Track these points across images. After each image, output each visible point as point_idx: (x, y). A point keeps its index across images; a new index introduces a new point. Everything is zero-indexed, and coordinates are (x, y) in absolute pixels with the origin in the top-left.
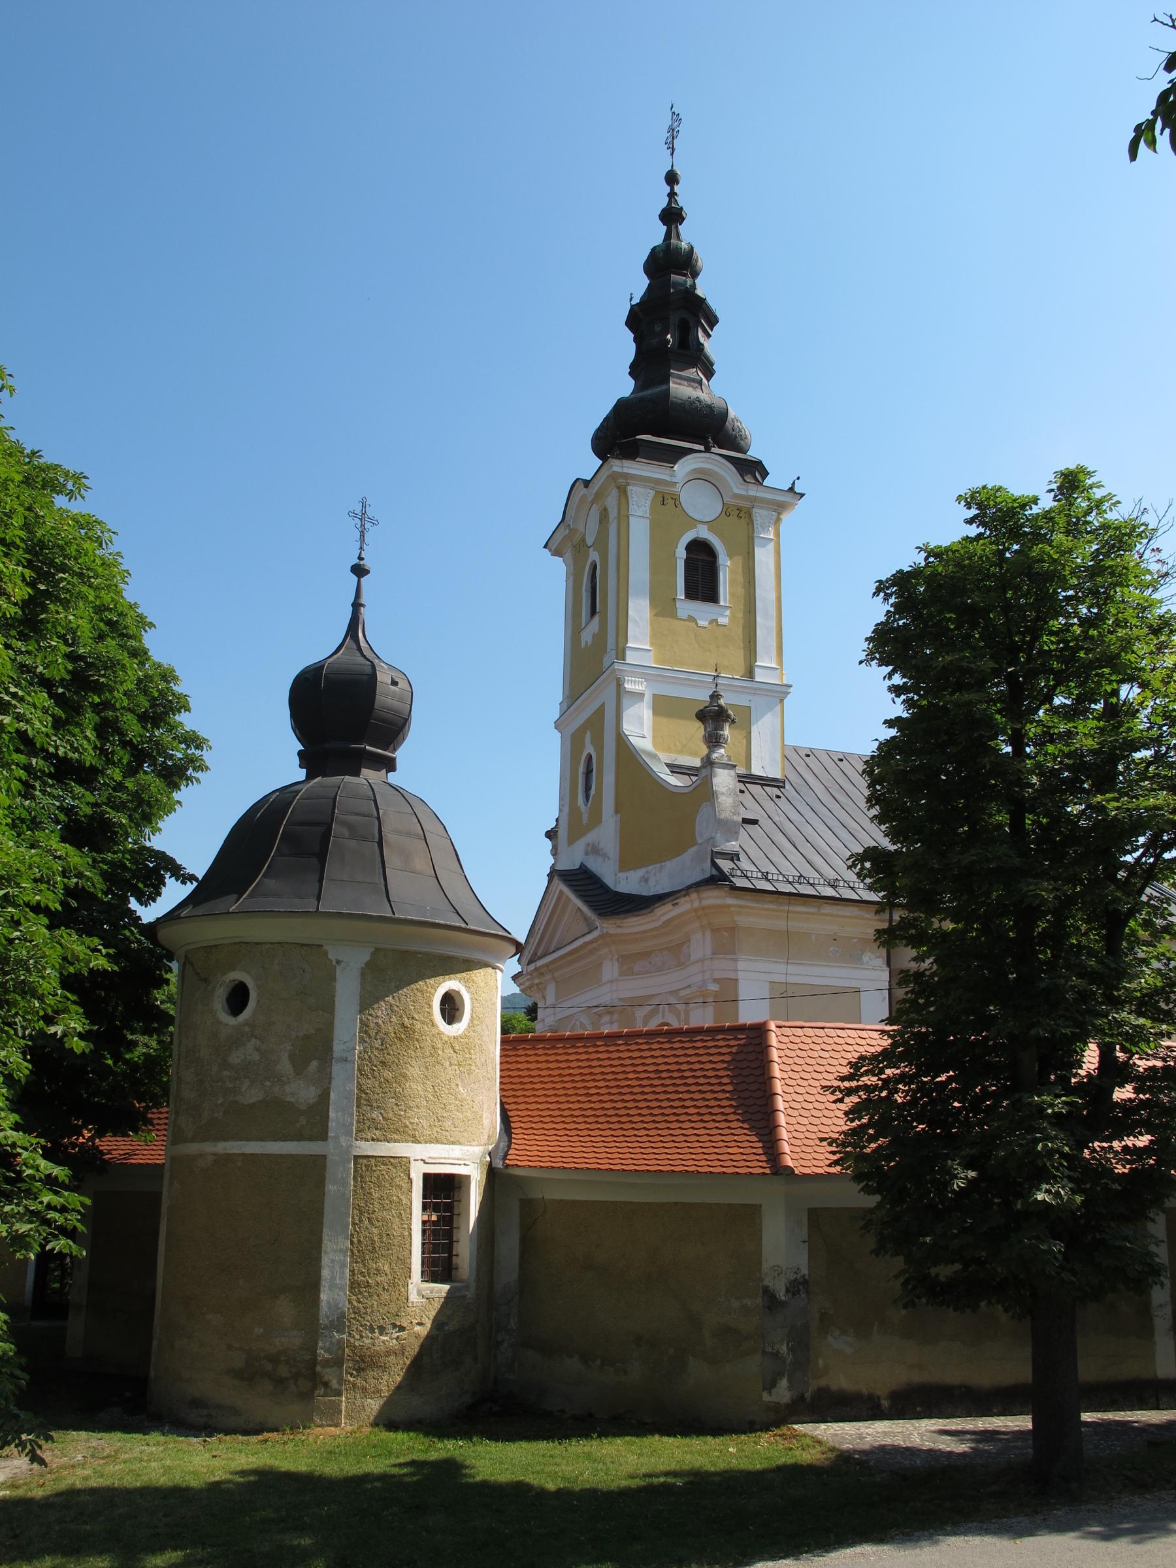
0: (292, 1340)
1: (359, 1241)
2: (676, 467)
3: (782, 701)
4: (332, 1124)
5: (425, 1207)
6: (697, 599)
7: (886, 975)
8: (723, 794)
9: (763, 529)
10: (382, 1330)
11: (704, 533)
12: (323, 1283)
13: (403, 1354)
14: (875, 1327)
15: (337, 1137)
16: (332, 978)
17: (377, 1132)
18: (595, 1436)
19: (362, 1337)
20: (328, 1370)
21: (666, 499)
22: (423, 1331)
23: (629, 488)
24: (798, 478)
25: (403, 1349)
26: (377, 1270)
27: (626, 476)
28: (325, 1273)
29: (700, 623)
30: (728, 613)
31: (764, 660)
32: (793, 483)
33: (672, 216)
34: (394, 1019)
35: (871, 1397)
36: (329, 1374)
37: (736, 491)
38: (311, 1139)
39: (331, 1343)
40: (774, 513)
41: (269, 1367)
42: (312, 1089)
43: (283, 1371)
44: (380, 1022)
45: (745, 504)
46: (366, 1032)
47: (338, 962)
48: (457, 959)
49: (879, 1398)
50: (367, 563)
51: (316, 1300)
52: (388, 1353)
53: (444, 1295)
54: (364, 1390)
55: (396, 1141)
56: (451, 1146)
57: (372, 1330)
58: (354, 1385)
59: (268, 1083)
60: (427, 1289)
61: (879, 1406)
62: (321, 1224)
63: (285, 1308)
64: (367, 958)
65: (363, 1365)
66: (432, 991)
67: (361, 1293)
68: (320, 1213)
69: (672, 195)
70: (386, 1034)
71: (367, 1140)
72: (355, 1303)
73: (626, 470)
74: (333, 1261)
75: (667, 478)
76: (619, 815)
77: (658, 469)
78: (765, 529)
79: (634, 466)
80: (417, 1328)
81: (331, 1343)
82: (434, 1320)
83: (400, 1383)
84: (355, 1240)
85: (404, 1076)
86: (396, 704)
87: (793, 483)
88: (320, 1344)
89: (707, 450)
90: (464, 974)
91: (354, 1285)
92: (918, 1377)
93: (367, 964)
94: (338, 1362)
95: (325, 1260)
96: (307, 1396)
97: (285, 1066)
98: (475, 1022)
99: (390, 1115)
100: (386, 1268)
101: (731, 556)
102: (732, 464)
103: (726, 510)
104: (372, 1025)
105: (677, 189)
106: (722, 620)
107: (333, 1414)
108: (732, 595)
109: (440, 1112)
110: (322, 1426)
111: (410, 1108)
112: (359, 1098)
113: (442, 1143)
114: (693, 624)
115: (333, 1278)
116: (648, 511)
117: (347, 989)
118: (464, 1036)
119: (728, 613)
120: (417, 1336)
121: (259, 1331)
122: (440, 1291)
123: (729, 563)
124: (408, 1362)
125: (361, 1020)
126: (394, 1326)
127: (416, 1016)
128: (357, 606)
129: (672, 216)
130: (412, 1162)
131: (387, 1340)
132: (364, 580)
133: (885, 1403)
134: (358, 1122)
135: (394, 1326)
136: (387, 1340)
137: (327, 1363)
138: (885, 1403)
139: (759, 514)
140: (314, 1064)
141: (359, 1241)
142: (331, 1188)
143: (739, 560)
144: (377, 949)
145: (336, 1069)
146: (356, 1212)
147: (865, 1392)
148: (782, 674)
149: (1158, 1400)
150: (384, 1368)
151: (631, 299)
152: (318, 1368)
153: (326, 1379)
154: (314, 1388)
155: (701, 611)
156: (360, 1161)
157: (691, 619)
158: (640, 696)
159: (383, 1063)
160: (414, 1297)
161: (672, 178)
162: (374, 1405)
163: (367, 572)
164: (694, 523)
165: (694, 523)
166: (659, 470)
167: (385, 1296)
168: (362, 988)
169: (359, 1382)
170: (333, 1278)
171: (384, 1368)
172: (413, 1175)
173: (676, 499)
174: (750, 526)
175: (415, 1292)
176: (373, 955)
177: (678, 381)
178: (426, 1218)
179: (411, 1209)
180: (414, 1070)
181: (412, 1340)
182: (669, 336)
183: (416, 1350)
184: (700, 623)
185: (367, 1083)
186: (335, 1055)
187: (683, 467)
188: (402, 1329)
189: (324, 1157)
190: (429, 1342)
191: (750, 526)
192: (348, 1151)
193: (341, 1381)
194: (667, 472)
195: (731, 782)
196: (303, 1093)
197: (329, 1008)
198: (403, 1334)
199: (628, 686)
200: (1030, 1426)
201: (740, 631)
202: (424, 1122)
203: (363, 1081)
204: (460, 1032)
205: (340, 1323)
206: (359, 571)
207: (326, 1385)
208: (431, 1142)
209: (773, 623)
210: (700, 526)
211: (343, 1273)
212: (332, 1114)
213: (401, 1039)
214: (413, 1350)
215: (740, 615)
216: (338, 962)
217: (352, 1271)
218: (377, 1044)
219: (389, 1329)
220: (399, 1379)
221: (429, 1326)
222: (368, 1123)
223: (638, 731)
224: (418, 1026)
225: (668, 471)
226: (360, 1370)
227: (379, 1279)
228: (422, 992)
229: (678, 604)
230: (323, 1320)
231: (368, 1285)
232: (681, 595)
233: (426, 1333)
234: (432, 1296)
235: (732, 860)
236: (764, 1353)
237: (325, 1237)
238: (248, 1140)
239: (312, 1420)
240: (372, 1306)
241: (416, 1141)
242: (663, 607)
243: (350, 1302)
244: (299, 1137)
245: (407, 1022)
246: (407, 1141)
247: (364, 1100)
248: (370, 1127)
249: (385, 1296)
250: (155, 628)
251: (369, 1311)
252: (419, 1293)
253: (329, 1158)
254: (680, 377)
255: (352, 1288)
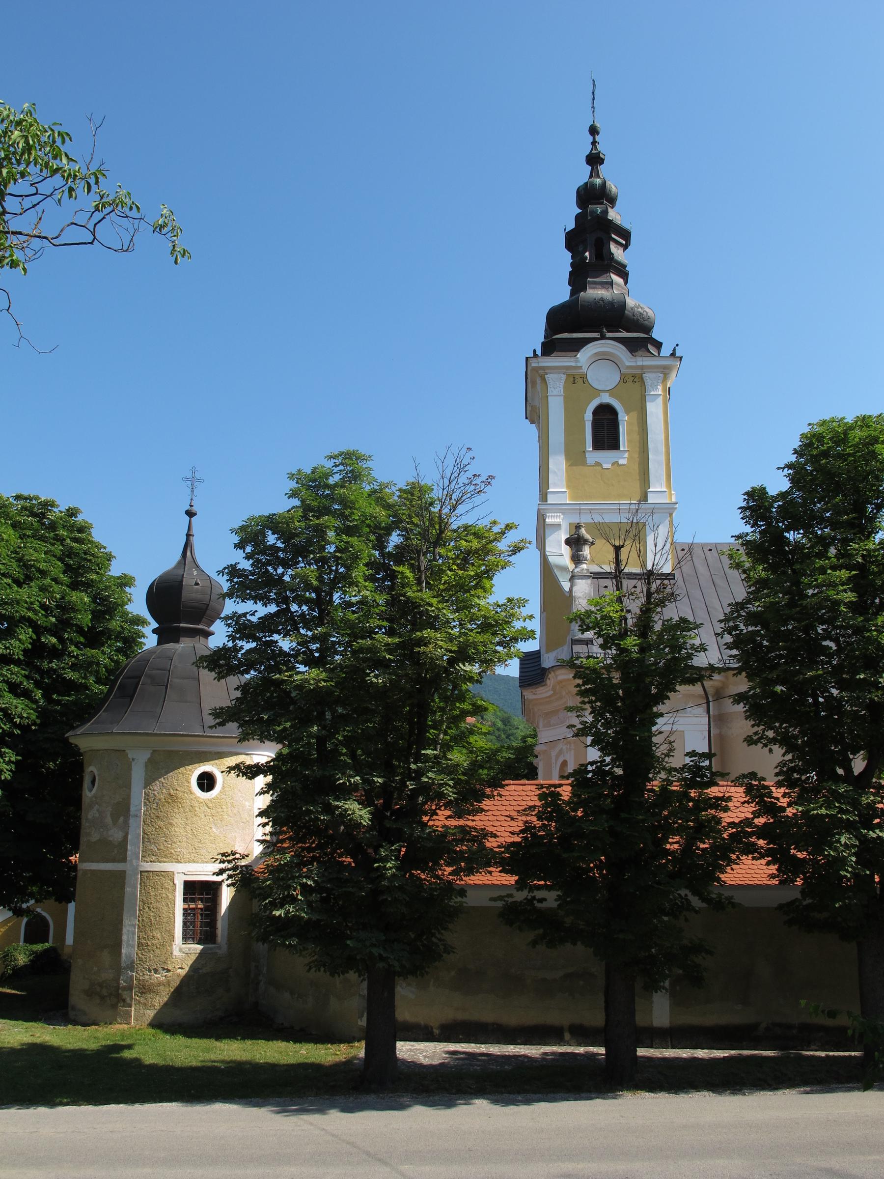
0: (107, 975)
1: (143, 920)
2: (578, 356)
3: (671, 515)
4: (129, 853)
5: (185, 900)
6: (603, 448)
7: (705, 720)
8: (580, 597)
9: (653, 388)
10: (156, 971)
11: (606, 399)
12: (123, 943)
13: (169, 985)
14: (432, 983)
15: (131, 860)
16: (130, 769)
17: (154, 857)
18: (239, 1038)
19: (144, 974)
20: (125, 992)
21: (576, 379)
22: (183, 972)
23: (546, 376)
24: (677, 345)
25: (169, 983)
26: (153, 937)
27: (543, 368)
28: (124, 938)
29: (605, 466)
30: (626, 455)
31: (657, 486)
32: (674, 350)
33: (594, 160)
34: (164, 791)
35: (426, 1027)
36: (125, 994)
37: (628, 364)
38: (119, 861)
39: (127, 977)
40: (661, 375)
41: (98, 989)
42: (120, 833)
43: (105, 992)
44: (156, 793)
45: (639, 371)
46: (148, 799)
47: (133, 759)
48: (210, 752)
49: (432, 1028)
50: (195, 509)
51: (120, 953)
52: (159, 984)
53: (198, 951)
54: (145, 1004)
55: (164, 862)
56: (205, 864)
57: (150, 971)
58: (139, 1002)
59: (102, 830)
60: (186, 948)
61: (432, 1033)
62: (123, 909)
63: (106, 957)
64: (149, 756)
65: (144, 990)
66: (190, 773)
67: (143, 950)
68: (122, 904)
69: (594, 143)
70: (159, 800)
71: (147, 862)
72: (140, 955)
73: (541, 365)
74: (128, 931)
75: (573, 364)
76: (545, 613)
77: (565, 359)
78: (655, 387)
79: (550, 360)
80: (179, 971)
81: (127, 977)
82: (190, 967)
83: (167, 1001)
84: (140, 919)
85: (171, 824)
86: (199, 596)
87: (674, 350)
88: (121, 978)
89: (603, 337)
90: (216, 761)
91: (140, 945)
92: (461, 1016)
93: (149, 760)
94: (130, 988)
95: (124, 931)
96: (114, 1007)
97: (109, 820)
98: (226, 789)
99: (162, 847)
100: (159, 936)
101: (627, 412)
102: (619, 342)
103: (624, 379)
104: (151, 795)
105: (598, 138)
106: (621, 462)
107: (127, 1017)
108: (629, 441)
109: (197, 845)
110: (121, 1024)
111: (174, 843)
112: (143, 838)
113: (198, 862)
114: (599, 468)
115: (128, 941)
116: (562, 391)
117: (138, 774)
118: (217, 798)
119: (626, 455)
120: (179, 975)
121: (95, 969)
122: (196, 949)
123: (626, 418)
124: (172, 990)
125: (145, 792)
126: (164, 969)
127: (179, 789)
128: (189, 535)
129: (594, 160)
130: (176, 875)
131: (160, 977)
132: (193, 519)
133: (436, 1031)
134: (143, 851)
135: (164, 969)
136: (160, 977)
137: (124, 988)
138: (436, 1031)
139: (648, 377)
140: (122, 819)
141: (143, 920)
142: (128, 889)
143: (634, 414)
144: (154, 751)
145: (132, 821)
146: (141, 903)
147: (422, 1023)
148: (671, 494)
149: (652, 1042)
150: (157, 993)
151: (565, 230)
152: (120, 991)
153: (124, 997)
154: (118, 1002)
155: (606, 458)
156: (143, 874)
157: (598, 464)
158: (558, 526)
159: (157, 817)
160: (176, 952)
161: (593, 131)
162: (150, 1014)
163: (195, 514)
164: (598, 392)
165: (598, 392)
166: (566, 360)
167: (157, 951)
168: (146, 774)
169: (142, 1000)
170: (128, 941)
171: (157, 993)
172: (176, 882)
173: (584, 378)
174: (643, 387)
175: (178, 949)
176: (152, 754)
177: (594, 286)
178: (186, 906)
179: (174, 901)
180: (178, 820)
181: (175, 977)
182: (587, 254)
183: (178, 983)
184: (605, 466)
185: (149, 829)
186: (131, 813)
187: (584, 355)
188: (168, 971)
189: (125, 871)
190: (186, 981)
191: (643, 387)
192: (137, 869)
193: (131, 998)
194: (572, 360)
195: (587, 589)
196: (116, 835)
197: (128, 786)
198: (169, 974)
199: (548, 520)
200: (399, 1044)
201: (636, 467)
202: (185, 851)
203: (146, 828)
204: (213, 796)
205: (131, 967)
206: (190, 514)
207: (124, 1001)
208: (189, 862)
209: (663, 458)
210: (602, 394)
211: (134, 938)
212: (129, 847)
213: (168, 803)
214: (176, 983)
215: (636, 456)
216: (133, 759)
217: (139, 937)
218: (154, 806)
219: (160, 970)
220: (166, 999)
221: (187, 969)
222: (148, 852)
223: (558, 551)
224: (180, 794)
225: (573, 359)
226: (142, 993)
227: (154, 942)
228: (183, 774)
229: (587, 455)
230: (123, 965)
231: (148, 945)
232: (590, 448)
233: (185, 973)
234: (189, 952)
235: (587, 645)
236: (360, 995)
237: (125, 917)
238: (93, 862)
239: (116, 1020)
240: (150, 957)
241: (178, 861)
242: (575, 458)
243: (137, 955)
244: (114, 861)
245: (172, 792)
246: (172, 862)
247: (147, 839)
248: (148, 854)
249: (157, 951)
250: (115, 557)
251: (148, 960)
252: (181, 950)
253: (127, 872)
254: (595, 283)
255: (138, 946)
